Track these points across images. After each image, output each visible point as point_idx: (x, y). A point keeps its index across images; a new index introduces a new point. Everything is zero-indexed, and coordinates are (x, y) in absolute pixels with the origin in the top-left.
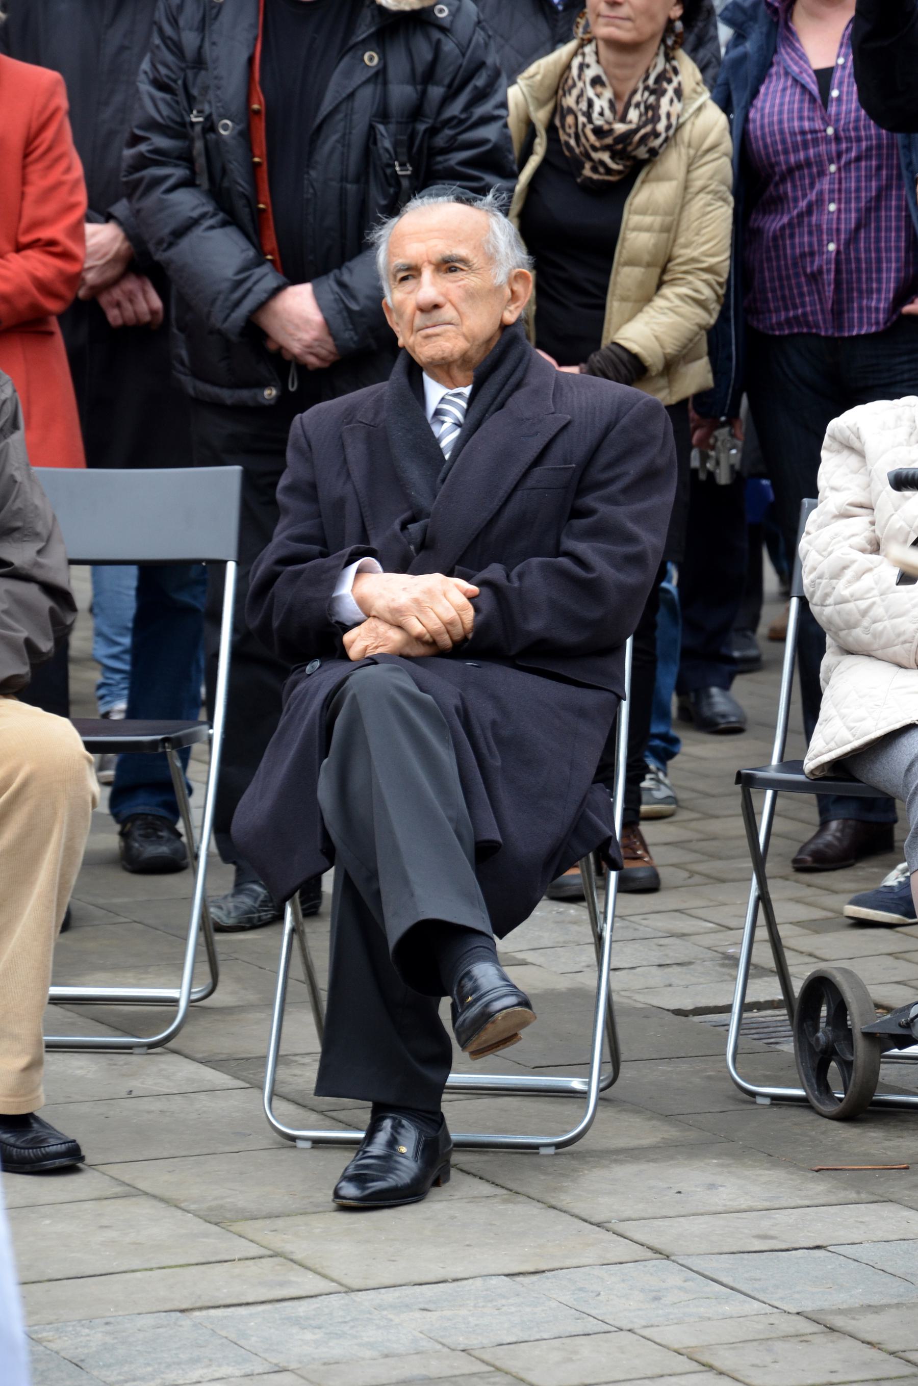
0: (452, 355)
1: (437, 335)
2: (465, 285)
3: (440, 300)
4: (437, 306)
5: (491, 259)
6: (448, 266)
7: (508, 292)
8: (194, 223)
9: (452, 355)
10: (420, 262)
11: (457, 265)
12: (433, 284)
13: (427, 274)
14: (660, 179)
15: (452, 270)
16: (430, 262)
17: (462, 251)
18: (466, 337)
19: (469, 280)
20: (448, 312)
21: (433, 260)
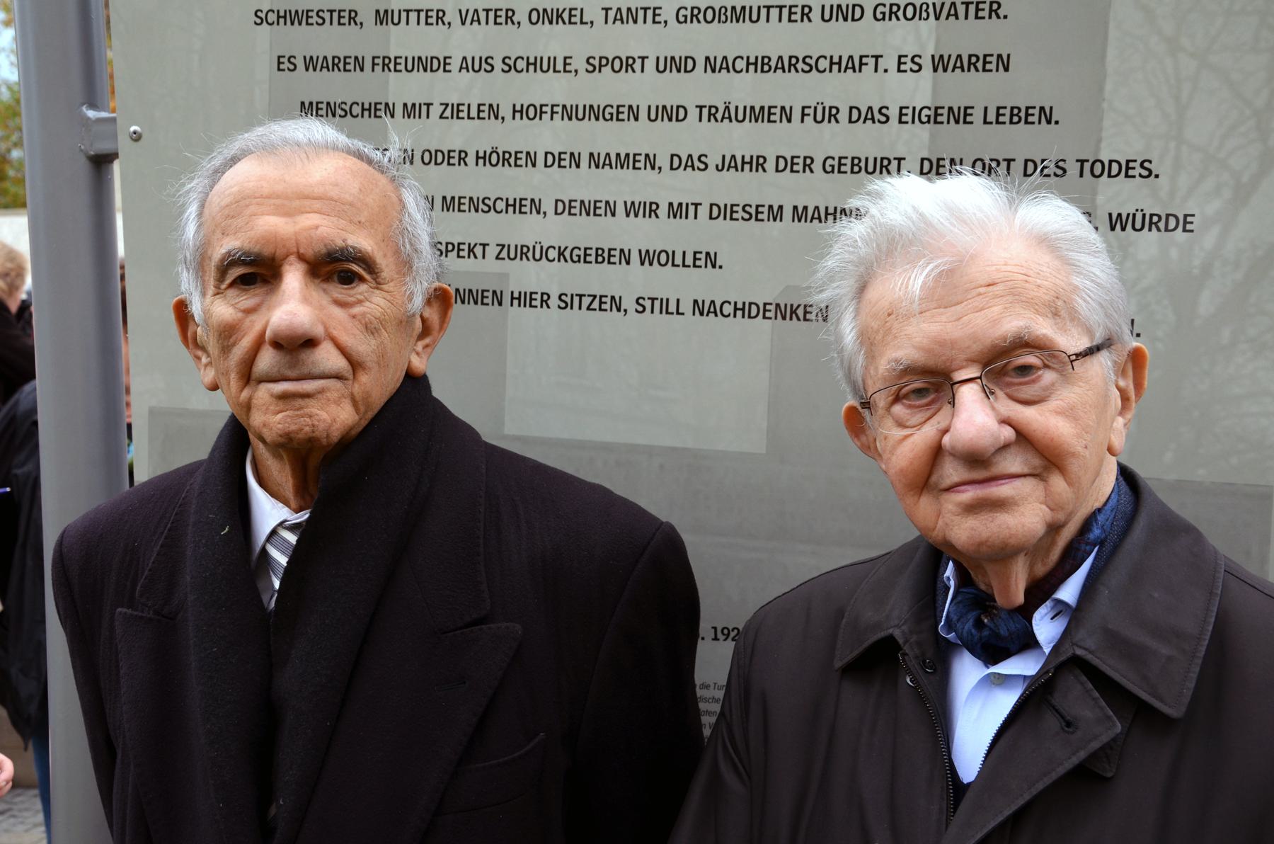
0: (328, 436)
1: (307, 396)
2: (364, 314)
3: (319, 331)
4: (310, 343)
5: (405, 265)
6: (336, 268)
7: (418, 323)
8: (1053, 384)
9: (327, 430)
10: (280, 253)
11: (355, 267)
12: (305, 300)
13: (293, 278)
14: (897, 361)
15: (348, 279)
16: (301, 258)
17: (362, 241)
18: (914, 347)
19: (373, 302)
20: (327, 357)
21: (309, 253)
